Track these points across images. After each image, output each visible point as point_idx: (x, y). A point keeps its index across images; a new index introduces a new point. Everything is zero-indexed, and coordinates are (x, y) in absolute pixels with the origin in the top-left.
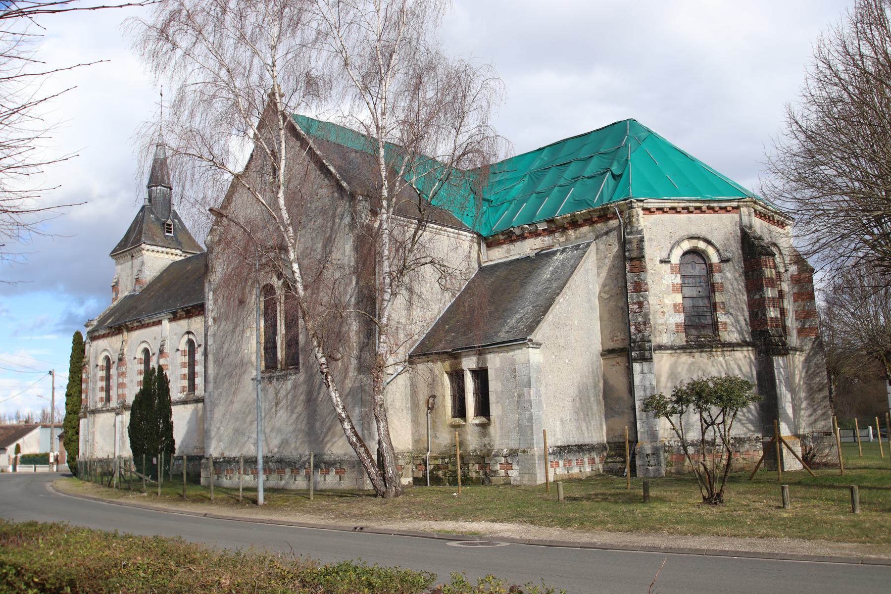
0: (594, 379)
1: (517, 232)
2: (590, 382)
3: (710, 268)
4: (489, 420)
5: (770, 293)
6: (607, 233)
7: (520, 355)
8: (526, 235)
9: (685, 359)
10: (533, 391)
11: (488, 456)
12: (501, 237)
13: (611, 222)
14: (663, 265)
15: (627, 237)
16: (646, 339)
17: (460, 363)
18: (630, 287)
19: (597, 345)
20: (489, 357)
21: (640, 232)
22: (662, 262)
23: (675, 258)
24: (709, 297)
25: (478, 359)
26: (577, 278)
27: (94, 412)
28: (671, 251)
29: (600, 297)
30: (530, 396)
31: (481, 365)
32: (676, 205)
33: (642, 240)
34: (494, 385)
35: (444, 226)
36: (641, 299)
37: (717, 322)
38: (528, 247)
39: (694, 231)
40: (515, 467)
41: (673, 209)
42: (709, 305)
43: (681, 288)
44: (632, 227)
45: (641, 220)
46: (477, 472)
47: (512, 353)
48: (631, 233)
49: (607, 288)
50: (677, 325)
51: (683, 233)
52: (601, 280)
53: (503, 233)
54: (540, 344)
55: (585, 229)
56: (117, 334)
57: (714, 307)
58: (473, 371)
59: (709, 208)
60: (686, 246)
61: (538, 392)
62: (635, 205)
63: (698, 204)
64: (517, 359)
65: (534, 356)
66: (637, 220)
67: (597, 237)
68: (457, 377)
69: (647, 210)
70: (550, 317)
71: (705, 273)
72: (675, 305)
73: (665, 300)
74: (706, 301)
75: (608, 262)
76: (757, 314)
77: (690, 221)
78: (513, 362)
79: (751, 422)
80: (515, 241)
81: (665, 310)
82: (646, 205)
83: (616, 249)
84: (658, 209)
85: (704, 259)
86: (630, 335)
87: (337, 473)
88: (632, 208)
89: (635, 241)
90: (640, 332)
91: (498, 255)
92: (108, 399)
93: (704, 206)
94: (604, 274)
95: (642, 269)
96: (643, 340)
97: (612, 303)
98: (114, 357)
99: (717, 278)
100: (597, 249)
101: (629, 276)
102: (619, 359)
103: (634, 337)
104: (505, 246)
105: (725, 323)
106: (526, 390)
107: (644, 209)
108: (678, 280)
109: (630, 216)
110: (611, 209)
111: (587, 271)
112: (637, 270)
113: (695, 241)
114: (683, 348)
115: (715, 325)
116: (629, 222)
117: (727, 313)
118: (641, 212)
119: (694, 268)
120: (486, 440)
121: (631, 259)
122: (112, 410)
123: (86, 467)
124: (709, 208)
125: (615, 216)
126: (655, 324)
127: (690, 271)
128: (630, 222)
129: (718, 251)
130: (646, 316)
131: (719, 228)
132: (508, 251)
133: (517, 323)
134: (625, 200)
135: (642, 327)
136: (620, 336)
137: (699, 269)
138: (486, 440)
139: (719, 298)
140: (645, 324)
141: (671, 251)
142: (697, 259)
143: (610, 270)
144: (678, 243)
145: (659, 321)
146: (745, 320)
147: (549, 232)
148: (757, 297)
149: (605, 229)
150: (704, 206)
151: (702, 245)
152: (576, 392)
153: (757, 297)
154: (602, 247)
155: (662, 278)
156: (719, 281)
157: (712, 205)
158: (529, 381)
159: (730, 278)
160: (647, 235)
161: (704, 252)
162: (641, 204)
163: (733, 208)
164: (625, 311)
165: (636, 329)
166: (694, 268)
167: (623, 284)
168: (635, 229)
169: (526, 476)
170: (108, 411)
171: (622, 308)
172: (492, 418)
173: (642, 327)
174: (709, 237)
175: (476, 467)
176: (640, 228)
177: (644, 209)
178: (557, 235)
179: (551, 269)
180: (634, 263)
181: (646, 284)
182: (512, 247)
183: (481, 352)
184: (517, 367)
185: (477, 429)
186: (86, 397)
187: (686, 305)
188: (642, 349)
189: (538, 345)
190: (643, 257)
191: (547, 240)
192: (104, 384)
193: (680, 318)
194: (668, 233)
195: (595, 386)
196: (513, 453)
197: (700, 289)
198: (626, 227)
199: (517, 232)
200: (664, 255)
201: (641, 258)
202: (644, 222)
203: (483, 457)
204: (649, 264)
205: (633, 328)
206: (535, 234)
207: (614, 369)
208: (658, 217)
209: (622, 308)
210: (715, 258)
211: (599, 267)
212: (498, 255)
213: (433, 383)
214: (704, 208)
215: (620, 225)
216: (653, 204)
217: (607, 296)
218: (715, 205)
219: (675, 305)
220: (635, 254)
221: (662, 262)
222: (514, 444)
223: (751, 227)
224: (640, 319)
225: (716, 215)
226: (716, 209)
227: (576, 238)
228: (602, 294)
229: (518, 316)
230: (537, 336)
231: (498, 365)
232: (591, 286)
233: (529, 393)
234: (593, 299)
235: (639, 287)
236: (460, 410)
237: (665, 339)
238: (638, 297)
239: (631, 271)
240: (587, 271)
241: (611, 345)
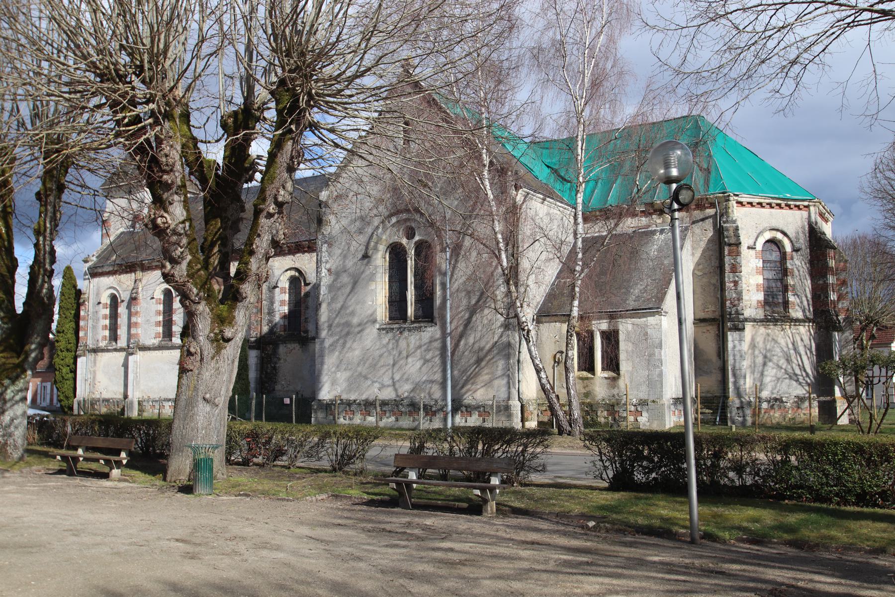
3: (783, 256)
4: (619, 374)
5: (831, 279)
6: (703, 220)
7: (651, 320)
9: (762, 330)
11: (618, 404)
14: (750, 250)
18: (727, 267)
21: (734, 222)
22: (749, 248)
23: (759, 246)
24: (781, 280)
27: (95, 351)
29: (694, 274)
31: (612, 328)
32: (762, 201)
33: (737, 229)
39: (774, 224)
40: (645, 414)
41: (760, 204)
44: (728, 217)
46: (605, 418)
48: (726, 222)
49: (701, 267)
50: (759, 302)
51: (766, 225)
53: (600, 211)
56: (127, 272)
57: (785, 288)
58: (603, 333)
60: (768, 235)
62: (731, 198)
63: (779, 202)
67: (694, 223)
69: (740, 203)
72: (757, 285)
73: (751, 281)
74: (779, 284)
75: (703, 245)
76: (820, 296)
77: (771, 215)
79: (809, 385)
81: (750, 288)
82: (740, 199)
84: (748, 203)
85: (779, 248)
87: (479, 416)
88: (729, 200)
90: (734, 306)
92: (114, 337)
93: (783, 203)
94: (698, 254)
95: (738, 254)
97: (705, 280)
98: (125, 296)
101: (727, 259)
102: (709, 328)
105: (793, 303)
107: (738, 202)
109: (727, 208)
113: (774, 232)
114: (761, 321)
115: (786, 304)
116: (725, 213)
117: (796, 294)
118: (735, 205)
119: (771, 255)
120: (615, 391)
121: (730, 245)
122: (121, 350)
123: (84, 405)
124: (787, 205)
128: (727, 212)
129: (791, 242)
131: (792, 222)
134: (723, 193)
136: (711, 308)
137: (775, 256)
138: (615, 391)
142: (774, 247)
143: (704, 251)
146: (808, 301)
147: (645, 213)
148: (821, 282)
149: (702, 217)
150: (783, 203)
151: (779, 236)
153: (821, 282)
159: (798, 265)
160: (739, 223)
161: (780, 241)
162: (736, 198)
163: (805, 207)
164: (722, 288)
166: (771, 255)
169: (656, 422)
170: (116, 350)
172: (622, 373)
173: (736, 302)
174: (785, 230)
175: (605, 413)
177: (738, 202)
178: (654, 216)
183: (612, 316)
184: (649, 331)
185: (606, 381)
186: (86, 334)
191: (644, 220)
192: (107, 322)
193: (761, 296)
196: (643, 403)
198: (722, 215)
200: (751, 243)
202: (738, 214)
203: (613, 406)
205: (728, 303)
207: (705, 335)
208: (748, 209)
214: (783, 205)
215: (716, 213)
216: (745, 199)
217: (700, 273)
219: (757, 285)
220: (733, 241)
222: (643, 395)
223: (816, 223)
225: (791, 211)
233: (660, 353)
235: (735, 269)
236: (588, 364)
239: (729, 255)
241: (702, 315)
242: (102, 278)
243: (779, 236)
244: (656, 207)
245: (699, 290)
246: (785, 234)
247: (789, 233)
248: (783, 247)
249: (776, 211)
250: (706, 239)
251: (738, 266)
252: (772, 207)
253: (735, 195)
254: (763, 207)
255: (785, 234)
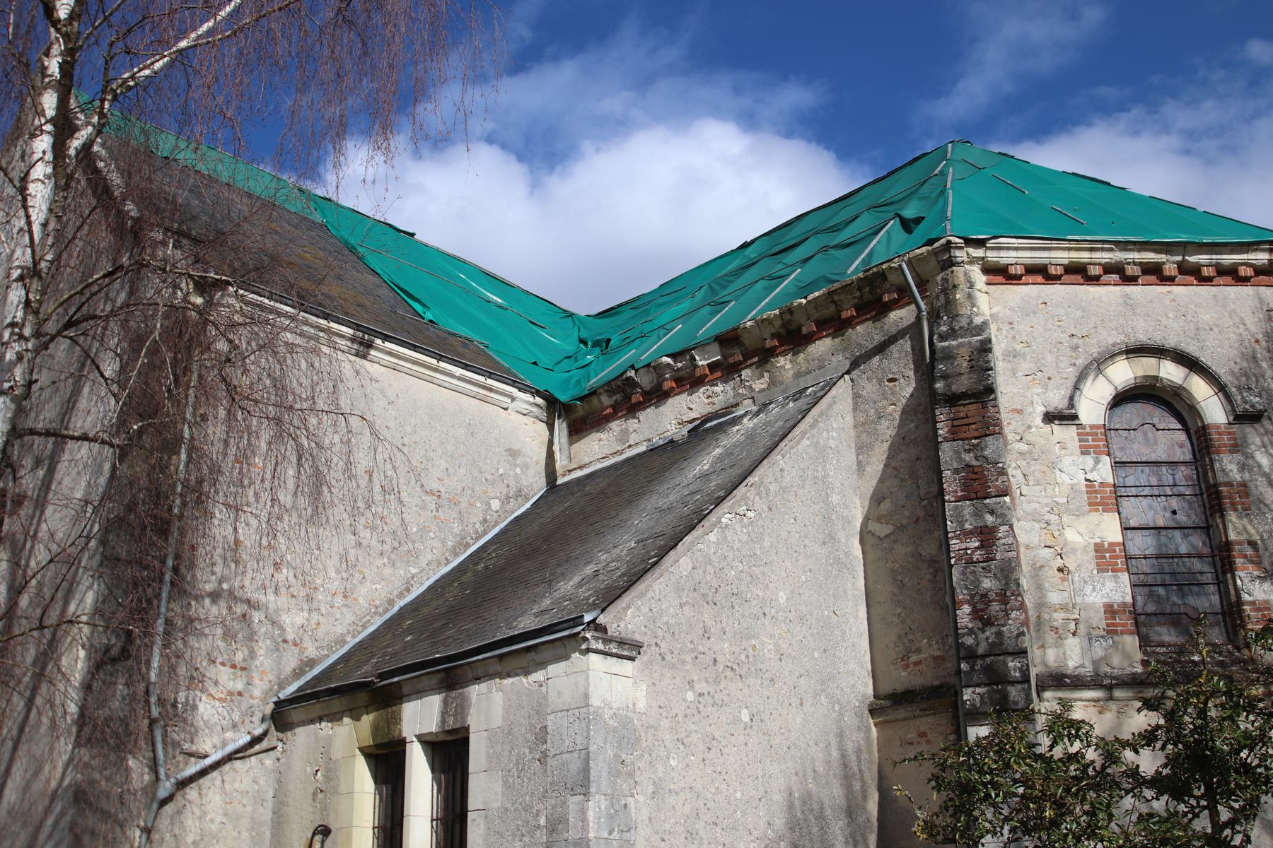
0: (848, 786)
1: (645, 380)
2: (834, 794)
6: (881, 348)
7: (557, 678)
8: (667, 385)
10: (596, 807)
12: (606, 400)
13: (894, 315)
15: (940, 345)
16: (1009, 644)
17: (396, 719)
18: (951, 484)
19: (859, 683)
20: (475, 691)
22: (1050, 417)
23: (1093, 404)
25: (445, 703)
26: (786, 465)
28: (1076, 387)
29: (864, 535)
30: (585, 828)
31: (451, 724)
32: (1084, 256)
33: (985, 348)
34: (483, 789)
35: (440, 358)
36: (990, 519)
37: (1239, 602)
38: (669, 418)
39: (1143, 333)
42: (1207, 551)
43: (1109, 498)
44: (954, 317)
45: (982, 301)
47: (539, 676)
48: (952, 333)
49: (886, 506)
50: (1110, 610)
51: (1113, 338)
52: (869, 484)
54: (637, 647)
55: (822, 346)
57: (1222, 558)
59: (1184, 269)
60: (1123, 373)
61: (619, 816)
62: (960, 255)
64: (552, 695)
65: (600, 681)
66: (970, 296)
67: (855, 364)
68: (387, 763)
70: (681, 563)
71: (1189, 457)
72: (1099, 549)
74: (1197, 540)
75: (887, 429)
78: (540, 709)
80: (641, 406)
81: (1071, 563)
82: (992, 256)
83: (910, 390)
86: (957, 636)
89: (964, 353)
90: (988, 622)
91: (600, 450)
93: (1170, 263)
95: (990, 427)
96: (999, 649)
97: (901, 550)
99: (1229, 467)
100: (856, 396)
102: (925, 723)
103: (969, 641)
104: (615, 426)
106: (574, 801)
108: (1104, 472)
109: (949, 289)
110: (892, 278)
111: (821, 452)
112: (972, 430)
113: (1151, 361)
116: (944, 306)
118: (980, 279)
121: (953, 400)
124: (1184, 269)
125: (904, 296)
126: (1041, 605)
127: (1138, 449)
128: (950, 304)
130: (1008, 572)
132: (625, 433)
133: (286, 343)
134: (930, 242)
135: (995, 607)
136: (929, 649)
139: (1237, 527)
140: (1003, 598)
141: (1076, 387)
144: (1099, 364)
145: (1054, 598)
147: (725, 370)
149: (878, 338)
150: (1170, 263)
151: (1171, 372)
152: (780, 822)
154: (870, 389)
155: (1053, 466)
156: (1237, 476)
157: (1192, 259)
158: (586, 770)
162: (979, 253)
164: (939, 566)
165: (976, 614)
167: (934, 488)
168: (963, 322)
171: (932, 562)
174: (1192, 349)
176: (978, 320)
178: (746, 373)
179: (718, 451)
180: (962, 411)
181: (1003, 472)
182: (632, 423)
184: (551, 721)
187: (1134, 550)
188: (996, 678)
189: (628, 649)
190: (990, 390)
191: (721, 393)
193: (1118, 589)
194: (1064, 337)
195: (852, 811)
197: (1175, 503)
198: (934, 317)
199: (645, 380)
200: (1057, 400)
201: (985, 393)
202: (988, 303)
204: (1011, 425)
206: (691, 381)
209: (932, 562)
210: (1214, 411)
211: (861, 448)
212: (600, 450)
213: (328, 786)
214: (1170, 269)
216: (1014, 254)
217: (882, 530)
218: (1202, 258)
219: (1099, 549)
220: (963, 384)
221: (1050, 417)
224: (987, 584)
225: (1205, 291)
226: (1206, 272)
227: (798, 375)
228: (872, 526)
229: (589, 570)
230: (627, 618)
231: (497, 720)
232: (835, 499)
233: (583, 812)
234: (841, 536)
235: (983, 484)
237: (1072, 655)
238: (978, 514)
239: (954, 435)
240: (821, 452)
241: (901, 679)
242: (474, 802)
243: (1171, 372)
244: (748, 341)
245: (885, 589)
246: (1192, 364)
247: (1205, 359)
248: (1194, 410)
249: (1145, 293)
250: (895, 411)
251: (990, 473)
252: (1129, 280)
253: (969, 242)
254: (1094, 280)
255: (1192, 364)
